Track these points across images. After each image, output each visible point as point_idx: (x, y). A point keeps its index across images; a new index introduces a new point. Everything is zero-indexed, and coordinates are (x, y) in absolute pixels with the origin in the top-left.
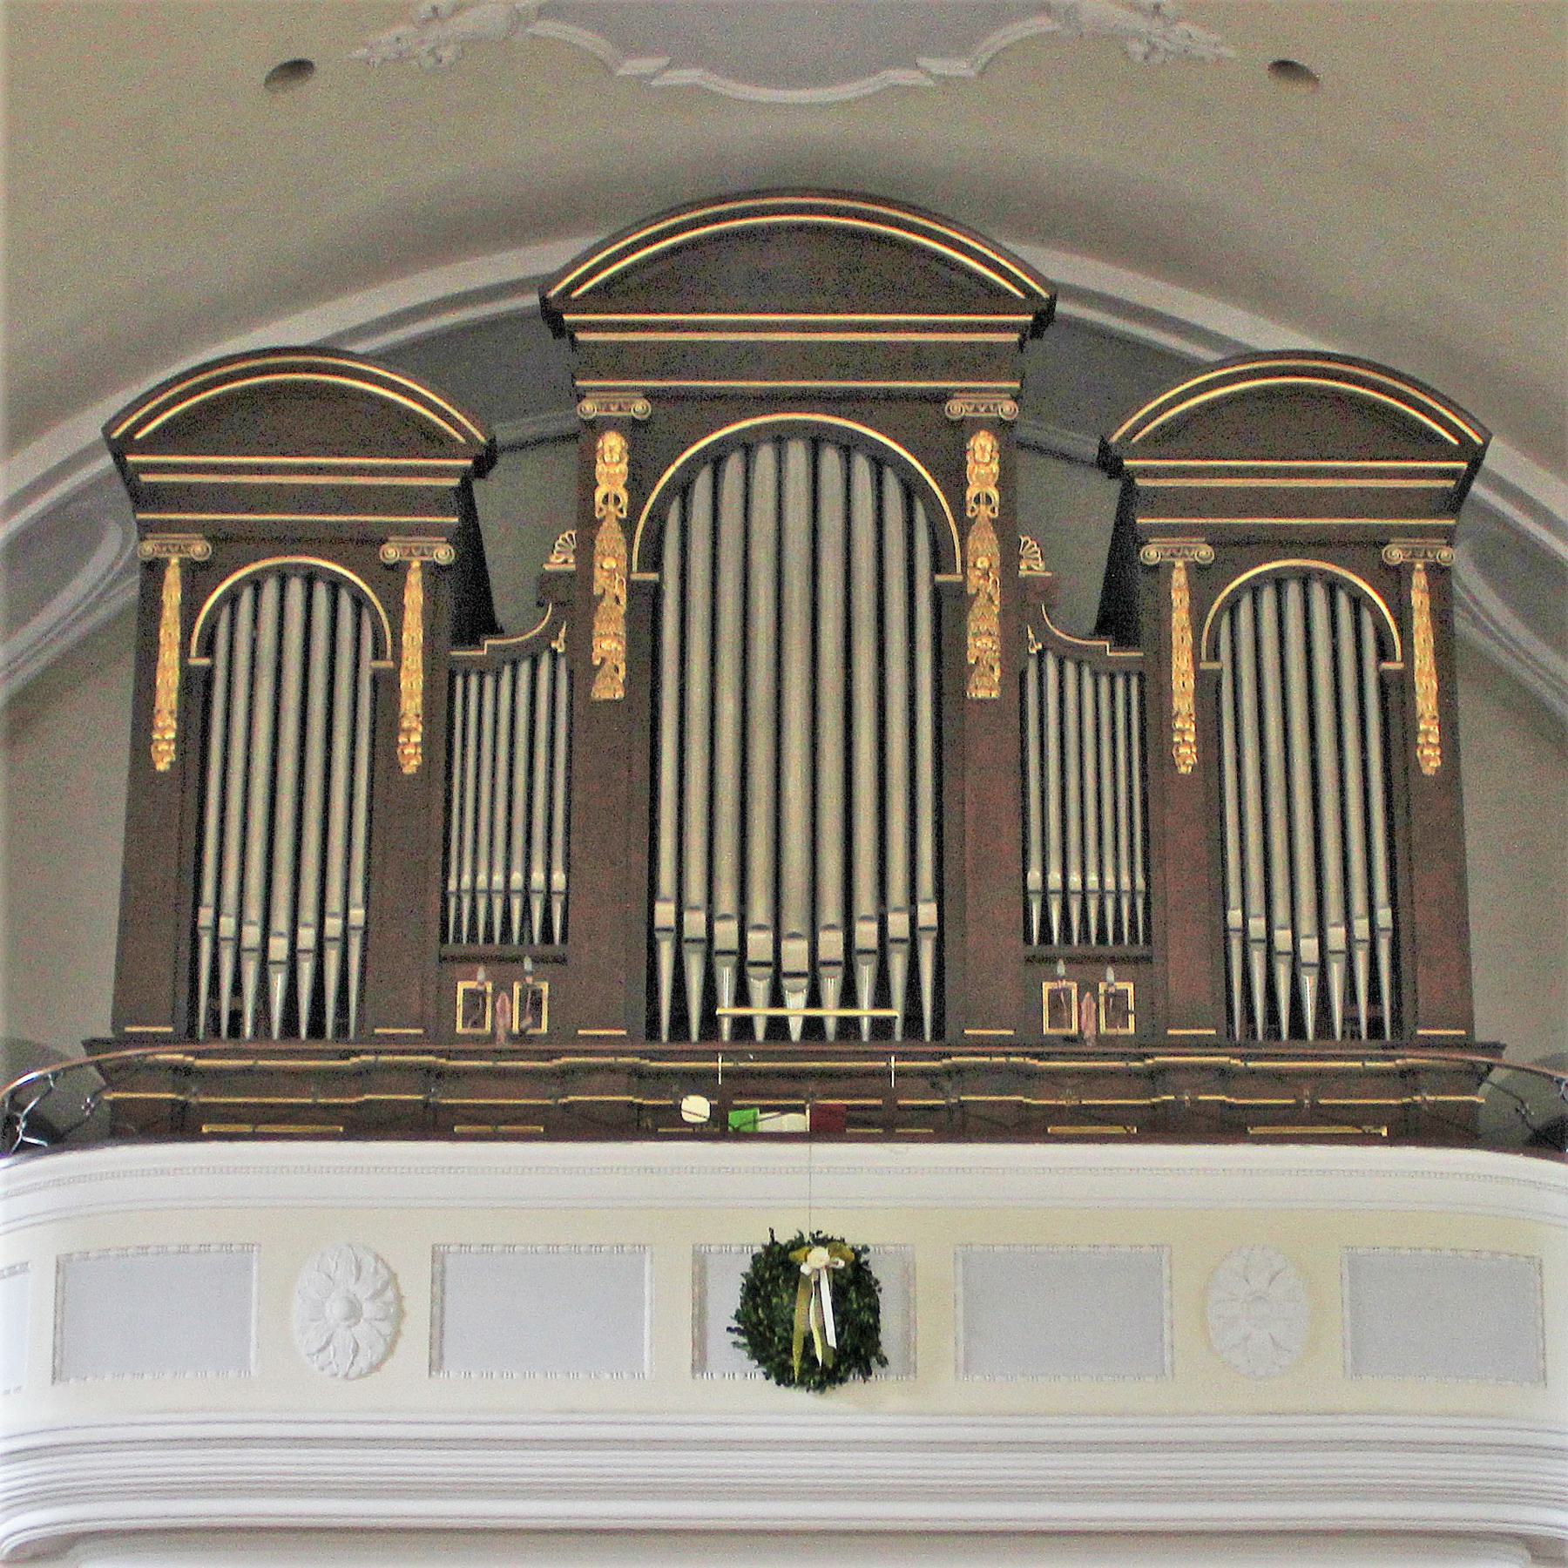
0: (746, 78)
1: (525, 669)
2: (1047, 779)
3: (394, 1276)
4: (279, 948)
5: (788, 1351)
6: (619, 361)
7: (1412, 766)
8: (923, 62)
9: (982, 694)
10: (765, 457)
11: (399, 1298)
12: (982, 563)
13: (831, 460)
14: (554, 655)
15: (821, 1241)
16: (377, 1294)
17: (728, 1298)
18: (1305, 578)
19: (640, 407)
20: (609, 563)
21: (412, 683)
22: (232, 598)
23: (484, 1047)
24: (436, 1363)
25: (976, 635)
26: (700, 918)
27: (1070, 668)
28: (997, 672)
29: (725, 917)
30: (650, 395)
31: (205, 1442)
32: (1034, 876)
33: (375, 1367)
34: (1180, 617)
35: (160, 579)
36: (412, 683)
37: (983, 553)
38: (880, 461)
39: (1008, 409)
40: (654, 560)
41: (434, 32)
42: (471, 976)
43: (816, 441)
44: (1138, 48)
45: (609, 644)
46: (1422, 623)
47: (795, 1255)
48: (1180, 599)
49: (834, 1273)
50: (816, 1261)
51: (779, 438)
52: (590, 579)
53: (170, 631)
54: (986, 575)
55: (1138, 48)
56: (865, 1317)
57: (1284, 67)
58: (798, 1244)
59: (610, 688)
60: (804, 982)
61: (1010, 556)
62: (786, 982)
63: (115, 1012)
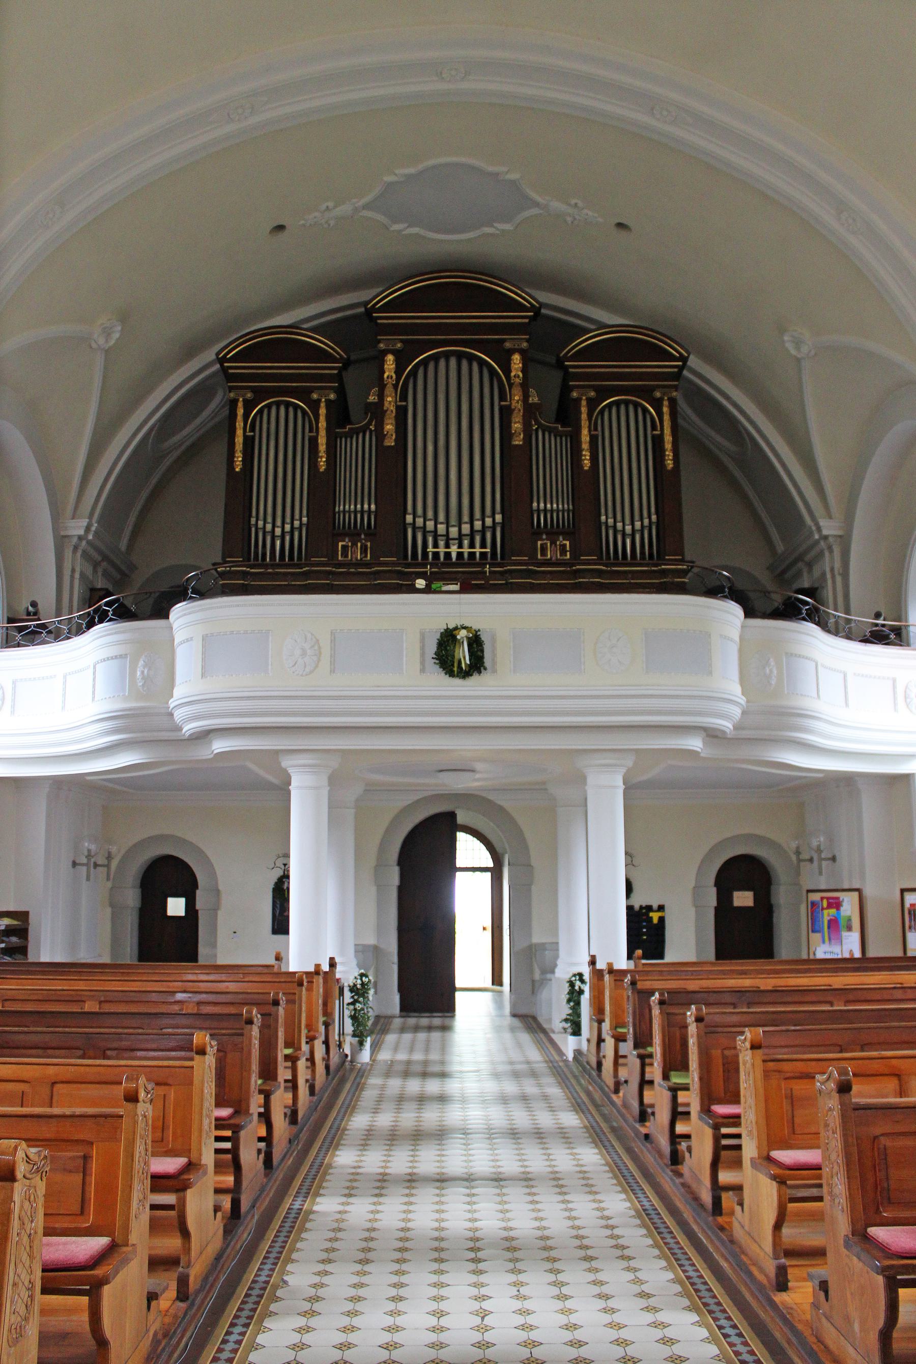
4: (278, 531)
5: (453, 665)
9: (517, 443)
10: (442, 363)
11: (320, 648)
12: (517, 398)
14: (371, 431)
15: (465, 628)
16: (313, 647)
17: (432, 647)
18: (627, 403)
20: (389, 399)
21: (322, 441)
22: (261, 412)
25: (515, 423)
28: (522, 436)
30: (401, 341)
32: (535, 505)
33: (311, 672)
34: (584, 416)
35: (236, 405)
36: (322, 441)
38: (482, 363)
40: (404, 397)
42: (344, 541)
43: (460, 356)
45: (389, 427)
46: (666, 418)
47: (456, 632)
48: (584, 410)
49: (468, 638)
50: (462, 634)
51: (447, 355)
52: (383, 405)
53: (239, 424)
56: (479, 653)
57: (620, 225)
58: (456, 628)
59: (390, 442)
60: (457, 541)
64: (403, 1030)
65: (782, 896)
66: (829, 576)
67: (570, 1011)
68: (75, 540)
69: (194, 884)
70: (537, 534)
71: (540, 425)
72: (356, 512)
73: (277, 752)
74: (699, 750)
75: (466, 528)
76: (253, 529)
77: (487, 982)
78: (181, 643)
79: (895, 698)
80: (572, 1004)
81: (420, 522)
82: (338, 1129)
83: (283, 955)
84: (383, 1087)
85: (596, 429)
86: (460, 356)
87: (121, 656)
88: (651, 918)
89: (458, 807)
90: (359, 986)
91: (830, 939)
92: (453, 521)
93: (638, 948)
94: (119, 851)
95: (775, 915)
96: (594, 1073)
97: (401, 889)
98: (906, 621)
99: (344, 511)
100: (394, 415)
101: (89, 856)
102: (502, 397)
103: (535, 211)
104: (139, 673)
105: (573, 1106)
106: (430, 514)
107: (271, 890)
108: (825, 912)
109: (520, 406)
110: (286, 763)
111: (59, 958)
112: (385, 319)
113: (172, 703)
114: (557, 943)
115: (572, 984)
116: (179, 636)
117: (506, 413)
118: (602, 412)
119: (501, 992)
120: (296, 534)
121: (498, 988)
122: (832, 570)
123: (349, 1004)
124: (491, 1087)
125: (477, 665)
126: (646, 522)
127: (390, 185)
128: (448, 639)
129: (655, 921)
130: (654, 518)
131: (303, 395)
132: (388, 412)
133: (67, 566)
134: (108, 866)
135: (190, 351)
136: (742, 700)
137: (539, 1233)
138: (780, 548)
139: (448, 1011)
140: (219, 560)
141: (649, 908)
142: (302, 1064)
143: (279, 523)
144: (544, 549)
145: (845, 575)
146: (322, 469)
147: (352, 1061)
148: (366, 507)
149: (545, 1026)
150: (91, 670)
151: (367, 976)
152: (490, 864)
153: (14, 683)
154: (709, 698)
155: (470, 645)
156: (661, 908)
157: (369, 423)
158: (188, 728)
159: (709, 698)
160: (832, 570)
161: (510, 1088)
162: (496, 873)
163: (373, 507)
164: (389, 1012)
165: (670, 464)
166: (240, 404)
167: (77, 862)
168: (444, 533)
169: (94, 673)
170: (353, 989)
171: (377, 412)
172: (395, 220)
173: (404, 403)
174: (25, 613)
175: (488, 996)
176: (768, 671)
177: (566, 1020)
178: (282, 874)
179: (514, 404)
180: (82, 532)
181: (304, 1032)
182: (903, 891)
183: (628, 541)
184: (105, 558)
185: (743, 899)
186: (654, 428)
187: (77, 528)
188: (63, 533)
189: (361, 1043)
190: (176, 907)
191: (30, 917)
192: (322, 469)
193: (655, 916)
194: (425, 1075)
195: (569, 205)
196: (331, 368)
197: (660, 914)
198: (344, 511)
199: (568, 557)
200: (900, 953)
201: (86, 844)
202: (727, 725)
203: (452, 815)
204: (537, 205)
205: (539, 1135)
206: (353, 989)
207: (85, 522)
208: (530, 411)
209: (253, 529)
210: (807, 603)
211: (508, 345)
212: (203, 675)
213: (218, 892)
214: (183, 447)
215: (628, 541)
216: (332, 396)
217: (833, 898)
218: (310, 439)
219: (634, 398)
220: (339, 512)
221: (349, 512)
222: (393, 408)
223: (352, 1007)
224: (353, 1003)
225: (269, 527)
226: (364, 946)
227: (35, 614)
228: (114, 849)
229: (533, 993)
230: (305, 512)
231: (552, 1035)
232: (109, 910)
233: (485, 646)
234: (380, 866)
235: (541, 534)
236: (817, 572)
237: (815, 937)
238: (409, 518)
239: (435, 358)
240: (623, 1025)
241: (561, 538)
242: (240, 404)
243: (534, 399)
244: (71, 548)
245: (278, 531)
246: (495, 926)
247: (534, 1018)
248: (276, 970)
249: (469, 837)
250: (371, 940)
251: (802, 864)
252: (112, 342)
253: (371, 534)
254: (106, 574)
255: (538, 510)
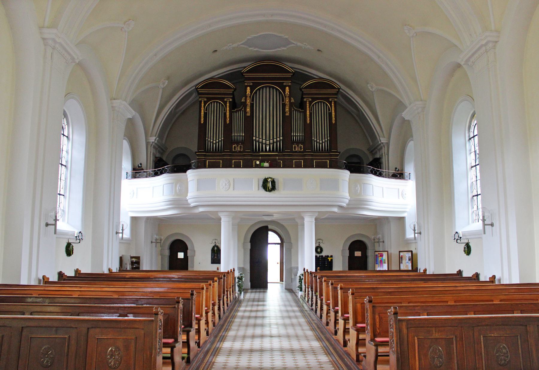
0: (263, 49)
1: (239, 112)
2: (294, 123)
3: (229, 181)
4: (214, 142)
5: (267, 188)
6: (249, 79)
7: (332, 122)
8: (281, 48)
9: (287, 115)
10: (265, 89)
11: (230, 183)
12: (287, 101)
13: (271, 89)
14: (243, 111)
15: (270, 178)
16: (228, 183)
17: (261, 183)
18: (321, 102)
19: (251, 84)
20: (248, 101)
21: (228, 114)
22: (209, 104)
23: (236, 152)
24: (234, 189)
25: (287, 109)
26: (258, 139)
27: (296, 112)
28: (289, 113)
29: (261, 139)
30: (252, 82)
31: (212, 197)
32: (292, 134)
33: (228, 190)
34: (308, 107)
35: (201, 103)
36: (228, 114)
37: (287, 100)
38: (277, 89)
39: (290, 84)
40: (253, 100)
41: (230, 47)
42: (235, 145)
43: (270, 87)
44: (303, 48)
45: (248, 110)
46: (333, 107)
47: (267, 179)
48: (308, 105)
49: (271, 181)
50: (270, 180)
51: (266, 87)
52: (246, 103)
53: (202, 109)
54: (287, 102)
55: (303, 48)
56: (274, 185)
57: (318, 50)
58: (268, 178)
59: (248, 114)
60: (269, 145)
61: (290, 100)
62: (267, 145)
63: (198, 149)
64: (252, 292)
65: (370, 254)
66: (384, 155)
67: (300, 285)
68: (151, 143)
69: (187, 248)
70: (293, 143)
71: (294, 109)
72: (238, 136)
73: (217, 211)
74: (336, 211)
75: (271, 141)
76: (207, 141)
77: (279, 281)
78: (190, 181)
79: (399, 195)
80: (300, 283)
81: (257, 139)
82: (224, 336)
83: (219, 268)
84: (241, 322)
85: (311, 111)
86: (270, 87)
87: (172, 183)
88: (328, 259)
89: (269, 225)
90: (240, 277)
91: (380, 266)
92: (268, 139)
93: (319, 267)
94: (164, 238)
95: (368, 259)
96: (304, 299)
97: (251, 250)
98: (404, 171)
99: (234, 136)
100: (250, 106)
101: (156, 240)
102: (283, 101)
103: (293, 45)
104: (177, 188)
105: (317, 339)
106: (261, 137)
107: (211, 250)
108: (379, 258)
109: (288, 103)
110: (220, 214)
111: (148, 269)
112: (247, 75)
113: (188, 198)
114: (298, 267)
115: (300, 277)
116: (189, 179)
117: (284, 105)
118: (313, 105)
119: (283, 283)
120: (220, 143)
121: (282, 282)
122: (385, 153)
123: (237, 282)
124: (280, 321)
125: (273, 188)
126: (326, 139)
127: (249, 39)
128: (265, 181)
129: (330, 260)
130: (329, 138)
131: (222, 99)
132: (248, 105)
133: (149, 151)
134: (160, 243)
135: (186, 84)
136: (349, 198)
137: (296, 366)
138: (371, 144)
139: (265, 288)
140: (197, 151)
141: (328, 256)
142: (203, 322)
143: (215, 139)
144: (295, 147)
145: (388, 155)
146: (228, 123)
147: (238, 298)
148: (241, 134)
149: (294, 291)
150: (162, 186)
151: (242, 274)
152: (280, 242)
153: (137, 189)
154: (337, 197)
155: (271, 183)
156: (332, 256)
157: (242, 108)
158: (192, 205)
159: (337, 197)
160: (385, 153)
161: (287, 321)
162: (282, 245)
163: (243, 134)
164: (247, 288)
165: (334, 122)
166: (203, 102)
167: (153, 241)
168: (265, 143)
169: (163, 187)
170: (238, 278)
171: (245, 105)
172: (250, 47)
173: (253, 102)
174: (138, 166)
175: (279, 284)
176: (357, 189)
177: (298, 287)
178: (214, 245)
179: (286, 103)
180: (154, 141)
181: (229, 287)
182: (400, 252)
183: (321, 145)
184: (159, 147)
185: (358, 254)
186: (329, 110)
187: (152, 139)
188: (148, 141)
189: (241, 293)
190: (181, 255)
191: (140, 258)
192: (228, 123)
193: (330, 259)
194: (258, 301)
195: (304, 44)
196: (231, 91)
197: (331, 258)
198: (234, 136)
199: (302, 150)
200: (399, 269)
201: (155, 236)
202: (344, 205)
203: (267, 227)
204: (294, 44)
205: (303, 351)
206: (238, 278)
207: (154, 138)
208: (291, 104)
209: (207, 141)
210: (371, 168)
211: (285, 84)
212: (197, 190)
213: (194, 251)
214: (182, 111)
215: (321, 145)
216: (231, 100)
217: (381, 254)
218: (224, 113)
219: (323, 101)
220: (233, 136)
221: (236, 136)
222: (249, 104)
223: (238, 283)
224: (238, 282)
225: (212, 140)
226: (240, 267)
227: (141, 167)
228: (162, 238)
229: (292, 282)
230: (222, 136)
231: (296, 293)
232: (160, 257)
233: (276, 183)
234: (244, 243)
235: (294, 143)
236: (381, 154)
237: (377, 265)
238: (254, 138)
239: (262, 88)
240: (329, 300)
241: (300, 145)
242: (203, 102)
243: (293, 101)
244: (150, 146)
245: (214, 142)
246: (281, 262)
247: (292, 290)
248: (217, 271)
249: (273, 233)
250: (242, 266)
251: (375, 243)
252: (165, 85)
253: (243, 142)
254: (159, 152)
255: (294, 136)
